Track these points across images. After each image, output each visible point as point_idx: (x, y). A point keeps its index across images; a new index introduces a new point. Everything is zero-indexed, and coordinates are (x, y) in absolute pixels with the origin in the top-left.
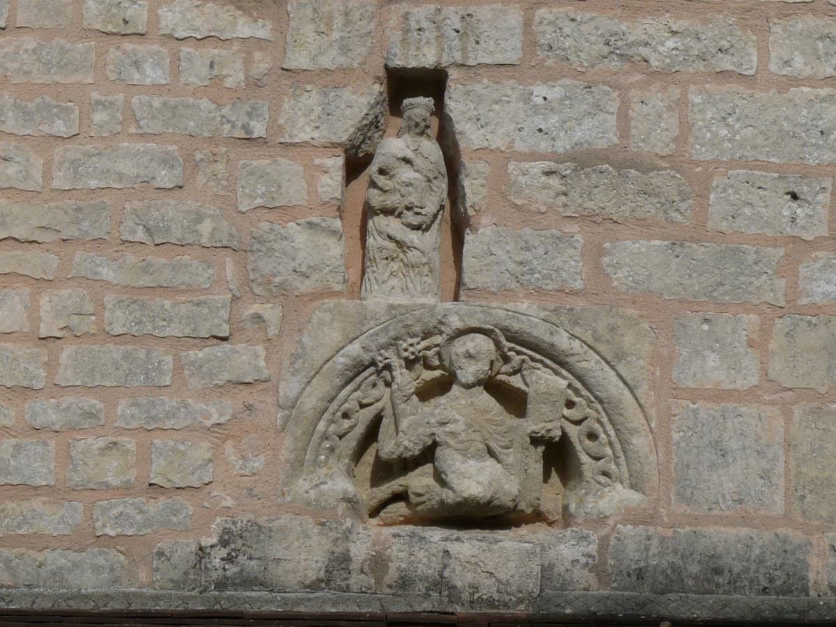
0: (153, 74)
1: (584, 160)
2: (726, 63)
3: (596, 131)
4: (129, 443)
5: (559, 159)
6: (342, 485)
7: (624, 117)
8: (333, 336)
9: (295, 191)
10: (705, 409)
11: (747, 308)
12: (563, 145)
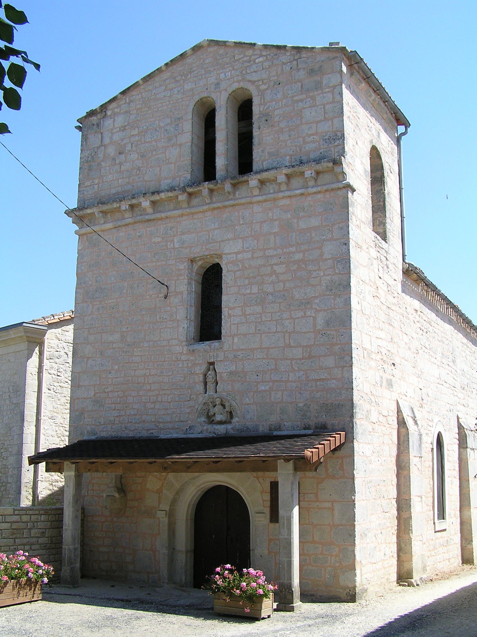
0: (180, 365)
1: (231, 373)
2: (249, 357)
3: (233, 368)
4: (178, 415)
5: (228, 372)
6: (203, 419)
7: (236, 366)
8: (201, 399)
9: (197, 380)
10: (246, 406)
11: (251, 392)
12: (229, 371)
